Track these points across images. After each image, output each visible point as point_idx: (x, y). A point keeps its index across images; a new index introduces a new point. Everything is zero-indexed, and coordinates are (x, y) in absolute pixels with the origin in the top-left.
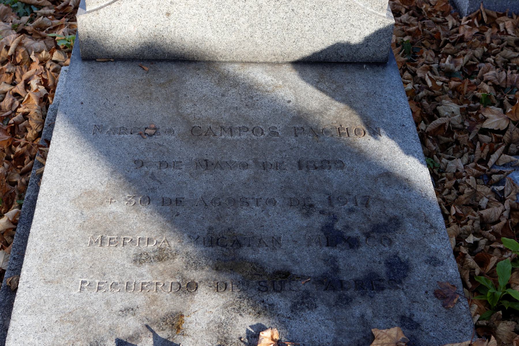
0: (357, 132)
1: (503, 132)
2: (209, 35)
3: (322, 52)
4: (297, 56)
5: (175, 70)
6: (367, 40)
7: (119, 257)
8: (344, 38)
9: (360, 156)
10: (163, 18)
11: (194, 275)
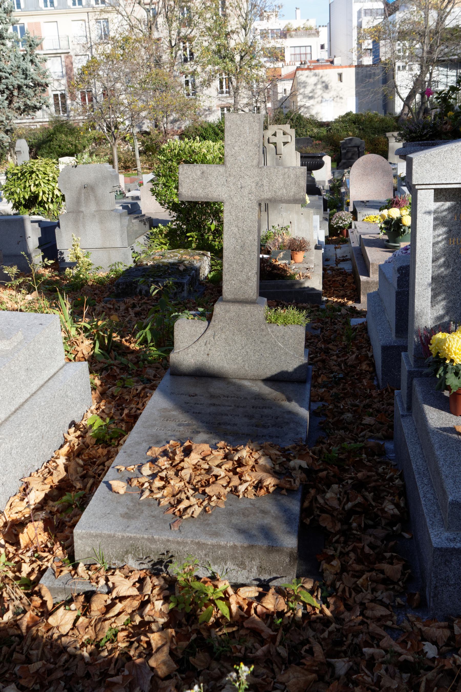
0: (283, 400)
1: (372, 426)
2: (225, 365)
3: (276, 375)
4: (264, 377)
5: (210, 379)
6: (296, 370)
7: (173, 424)
8: (285, 369)
9: (281, 406)
10: (205, 356)
11: (200, 430)
